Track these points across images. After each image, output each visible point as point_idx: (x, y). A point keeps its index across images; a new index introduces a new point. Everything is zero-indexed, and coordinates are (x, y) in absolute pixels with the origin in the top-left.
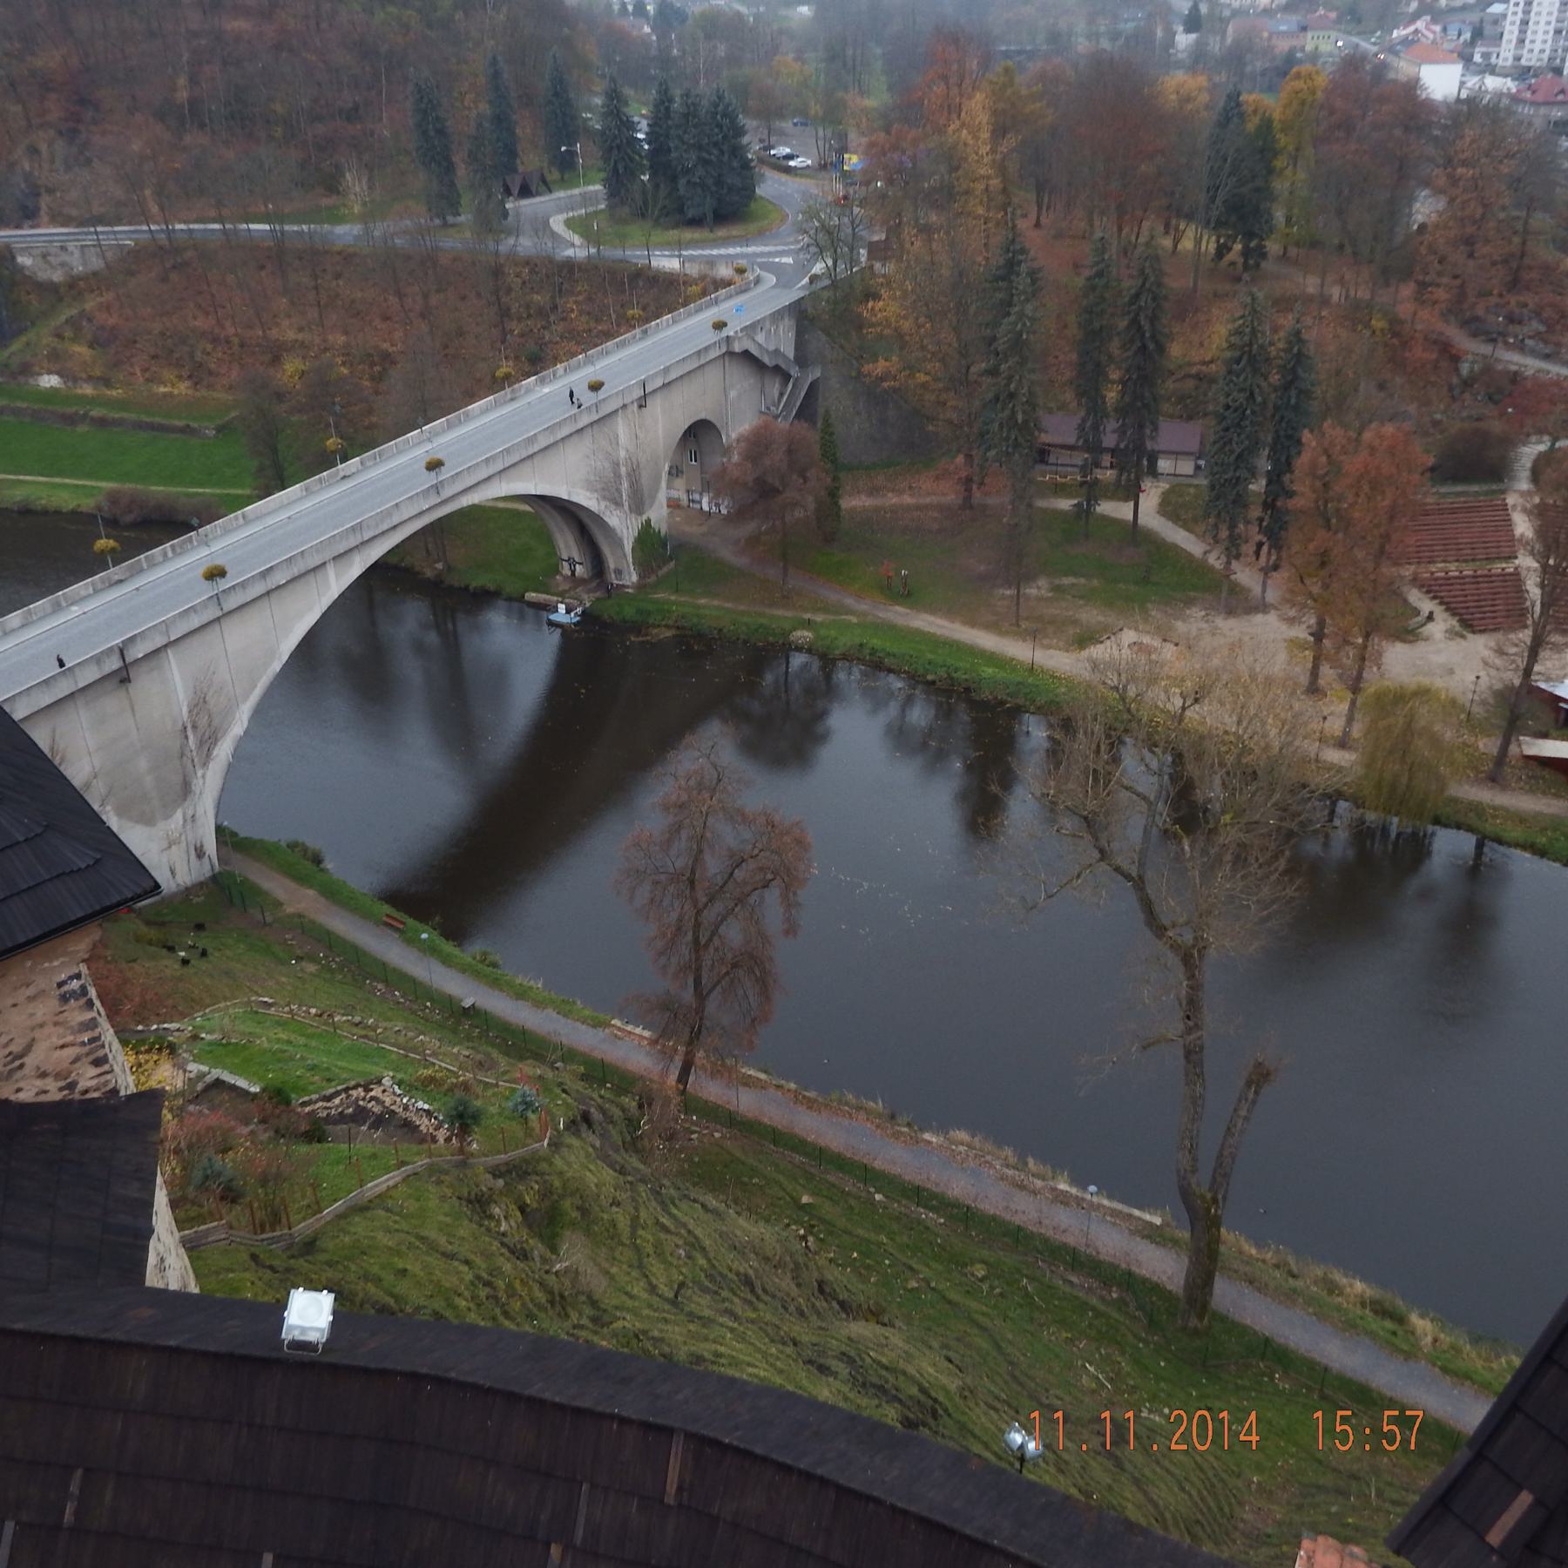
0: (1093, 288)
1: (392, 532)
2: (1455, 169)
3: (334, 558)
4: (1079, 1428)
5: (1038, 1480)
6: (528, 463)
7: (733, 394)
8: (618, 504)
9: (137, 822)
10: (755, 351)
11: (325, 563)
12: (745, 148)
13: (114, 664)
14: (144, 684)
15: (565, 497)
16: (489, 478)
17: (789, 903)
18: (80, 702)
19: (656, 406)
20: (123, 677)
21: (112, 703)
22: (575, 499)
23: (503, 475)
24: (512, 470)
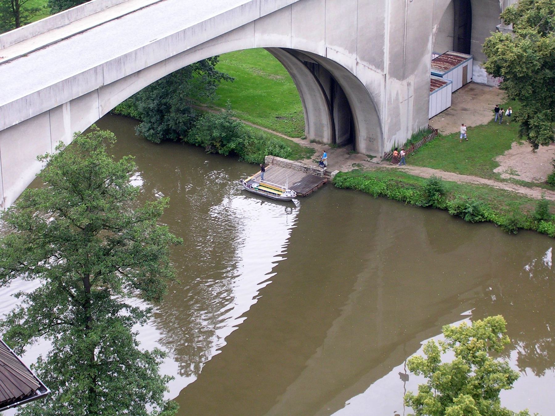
0: (287, 167)
1: (134, 79)
2: (510, 77)
3: (71, 101)
5: (412, 98)
6: (287, 14)
8: (379, 65)
11: (61, 106)
15: (322, 53)
16: (243, 27)
22: (331, 56)
23: (258, 26)
24: (269, 21)
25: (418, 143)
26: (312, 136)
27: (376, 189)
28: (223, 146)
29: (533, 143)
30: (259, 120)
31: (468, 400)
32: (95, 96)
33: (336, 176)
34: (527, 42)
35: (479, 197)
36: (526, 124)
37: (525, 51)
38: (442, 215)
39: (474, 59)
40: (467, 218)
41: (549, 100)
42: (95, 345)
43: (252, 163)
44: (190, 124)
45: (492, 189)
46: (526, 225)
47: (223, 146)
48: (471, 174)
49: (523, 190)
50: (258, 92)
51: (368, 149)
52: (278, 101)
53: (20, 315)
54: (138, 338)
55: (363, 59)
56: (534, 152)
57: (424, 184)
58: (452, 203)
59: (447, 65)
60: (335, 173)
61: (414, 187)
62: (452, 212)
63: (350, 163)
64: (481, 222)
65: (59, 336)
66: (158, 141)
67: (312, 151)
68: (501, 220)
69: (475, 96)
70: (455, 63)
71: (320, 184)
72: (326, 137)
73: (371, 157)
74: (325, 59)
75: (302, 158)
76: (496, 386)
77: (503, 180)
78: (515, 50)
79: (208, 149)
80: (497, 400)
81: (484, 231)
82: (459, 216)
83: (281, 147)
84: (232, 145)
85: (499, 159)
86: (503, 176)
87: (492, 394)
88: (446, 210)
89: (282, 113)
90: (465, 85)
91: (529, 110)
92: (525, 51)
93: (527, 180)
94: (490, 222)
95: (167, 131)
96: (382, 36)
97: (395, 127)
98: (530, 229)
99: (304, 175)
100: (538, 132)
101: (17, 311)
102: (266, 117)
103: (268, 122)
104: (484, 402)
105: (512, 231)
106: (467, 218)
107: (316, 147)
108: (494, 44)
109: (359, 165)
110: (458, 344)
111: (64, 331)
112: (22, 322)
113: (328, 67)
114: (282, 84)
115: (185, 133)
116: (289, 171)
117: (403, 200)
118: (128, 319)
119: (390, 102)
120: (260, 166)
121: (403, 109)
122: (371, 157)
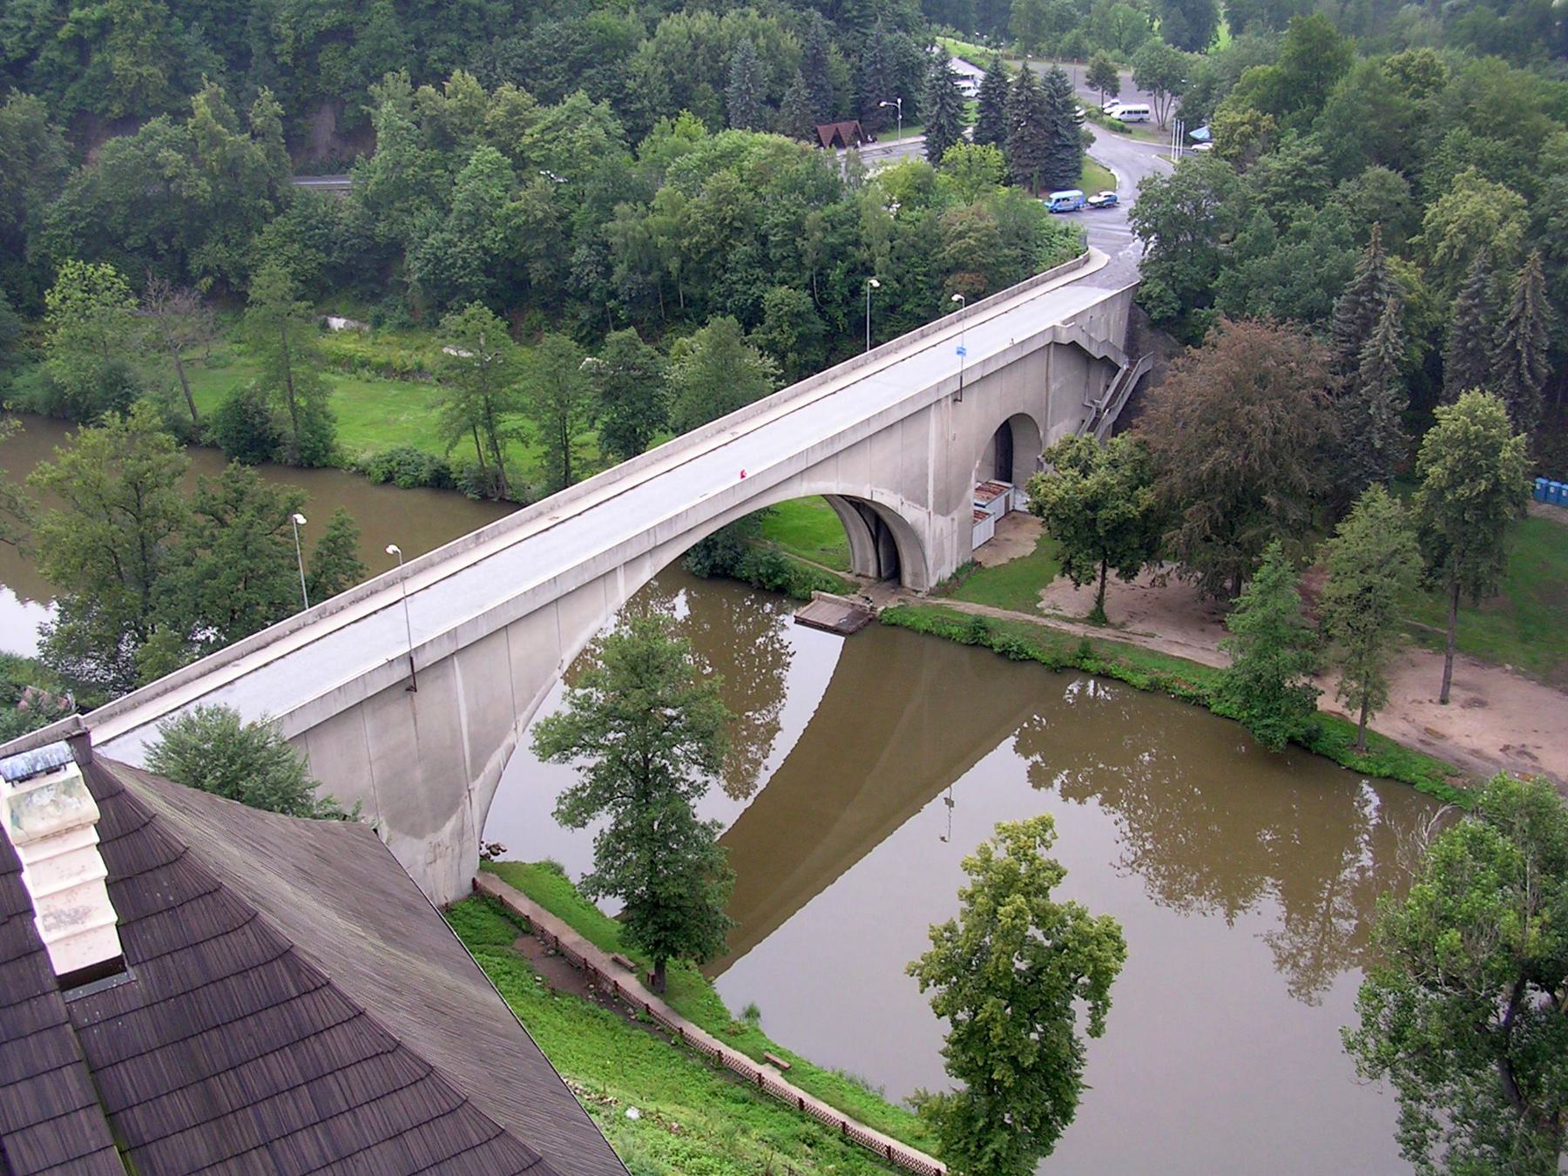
4: (1376, 194)
6: (833, 462)
7: (1054, 386)
8: (924, 504)
9: (407, 834)
10: (1084, 344)
11: (615, 569)
12: (1364, 171)
13: (402, 672)
14: (429, 692)
15: (867, 497)
17: (1097, 1013)
18: (367, 709)
19: (972, 400)
20: (409, 686)
21: (396, 711)
23: (805, 474)
24: (814, 469)
25: (963, 577)
26: (858, 571)
27: (923, 626)
28: (769, 581)
29: (1076, 580)
30: (805, 553)
31: (1020, 900)
32: (648, 556)
33: (883, 612)
34: (1067, 484)
35: (1023, 635)
36: (1068, 563)
37: (1067, 493)
38: (987, 652)
39: (1016, 487)
40: (1012, 656)
41: (1091, 540)
42: (654, 820)
43: (798, 599)
44: (736, 560)
45: (1036, 625)
46: (1070, 663)
47: (769, 581)
48: (1014, 610)
49: (1065, 627)
50: (804, 523)
51: (913, 583)
52: (822, 531)
53: (583, 789)
54: (695, 811)
55: (908, 499)
56: (1076, 589)
57: (969, 619)
58: (996, 641)
59: (989, 494)
60: (881, 609)
61: (959, 624)
62: (996, 649)
63: (896, 598)
64: (1024, 660)
65: (620, 810)
66: (706, 576)
67: (858, 586)
68: (1046, 658)
69: (1017, 525)
70: (997, 492)
71: (866, 619)
72: (872, 571)
73: (917, 592)
74: (871, 501)
75: (848, 593)
76: (1046, 884)
77: (1047, 616)
78: (1057, 492)
79: (756, 584)
80: (1046, 896)
81: (1028, 668)
82: (1004, 654)
83: (827, 582)
84: (779, 581)
85: (1041, 592)
86: (1046, 612)
87: (1042, 891)
88: (991, 647)
89: (828, 545)
90: (1007, 513)
91: (1071, 550)
92: (1067, 493)
93: (1070, 616)
94: (1034, 659)
95: (714, 566)
96: (927, 475)
97: (939, 562)
98: (1074, 667)
99: (850, 611)
100: (1080, 572)
101: (579, 786)
102: (812, 549)
103: (814, 554)
104: (1035, 900)
105: (1055, 670)
106: (1012, 656)
107: (860, 580)
108: (1036, 485)
109: (904, 601)
110: (1008, 841)
111: (626, 805)
112: (585, 795)
113: (873, 506)
114: (826, 514)
115: (732, 568)
116: (835, 607)
117: (949, 637)
118: (686, 793)
119: (934, 538)
120: (807, 600)
121: (947, 545)
122: (917, 592)
